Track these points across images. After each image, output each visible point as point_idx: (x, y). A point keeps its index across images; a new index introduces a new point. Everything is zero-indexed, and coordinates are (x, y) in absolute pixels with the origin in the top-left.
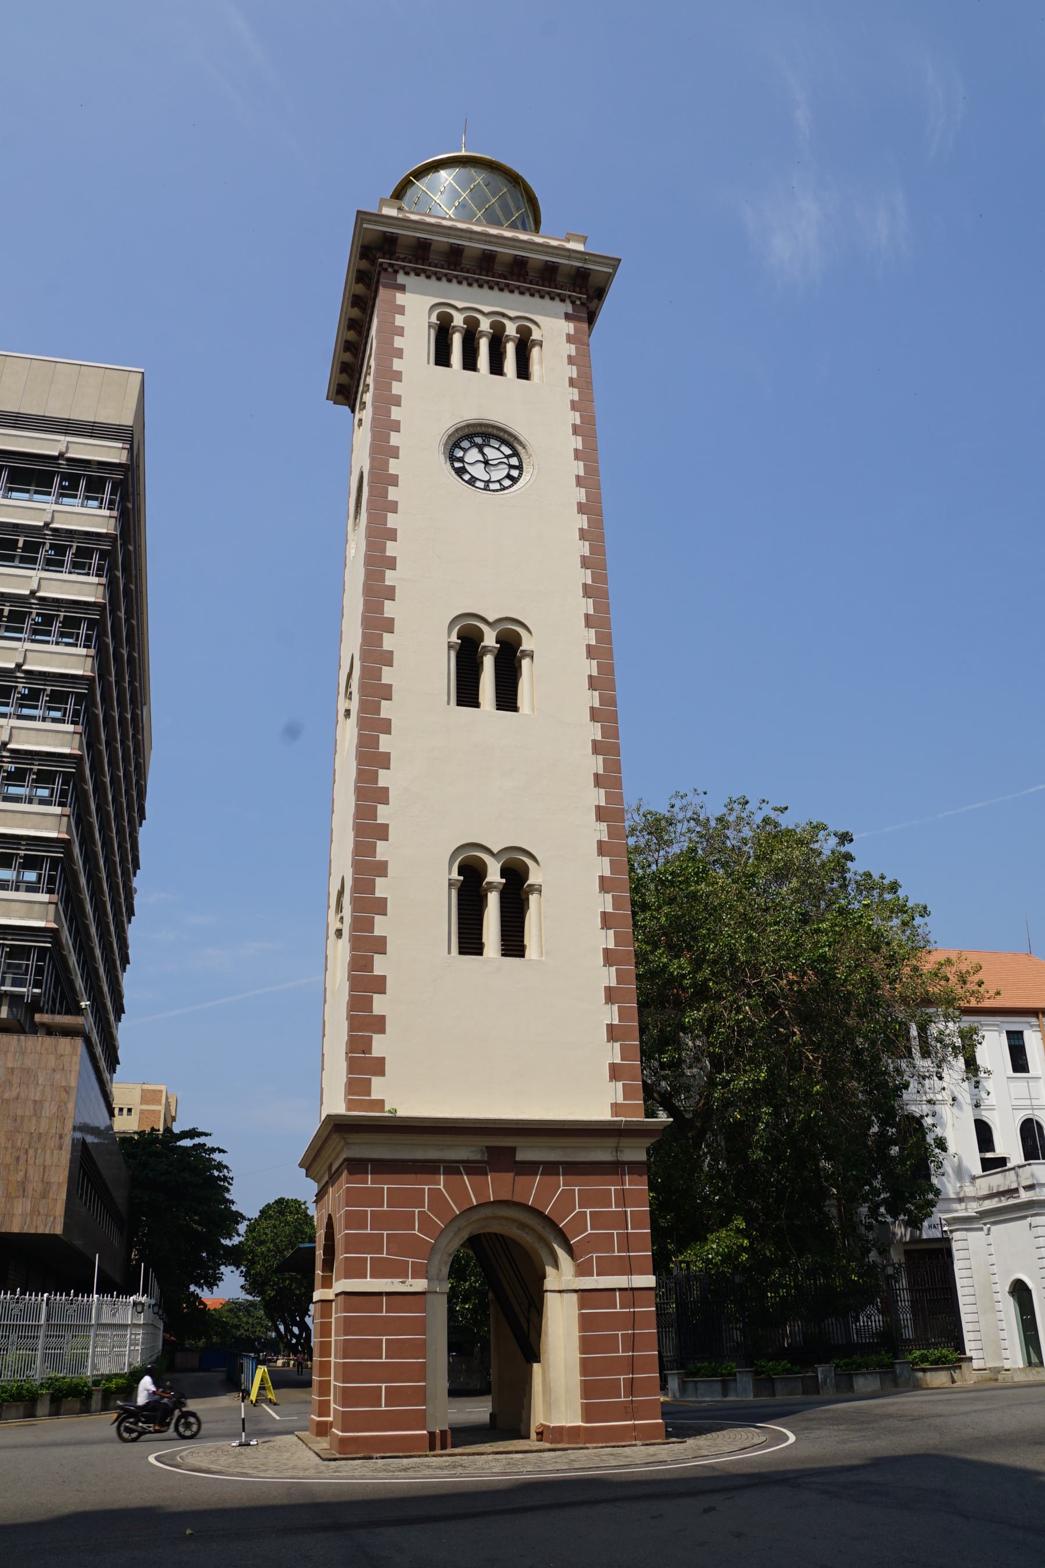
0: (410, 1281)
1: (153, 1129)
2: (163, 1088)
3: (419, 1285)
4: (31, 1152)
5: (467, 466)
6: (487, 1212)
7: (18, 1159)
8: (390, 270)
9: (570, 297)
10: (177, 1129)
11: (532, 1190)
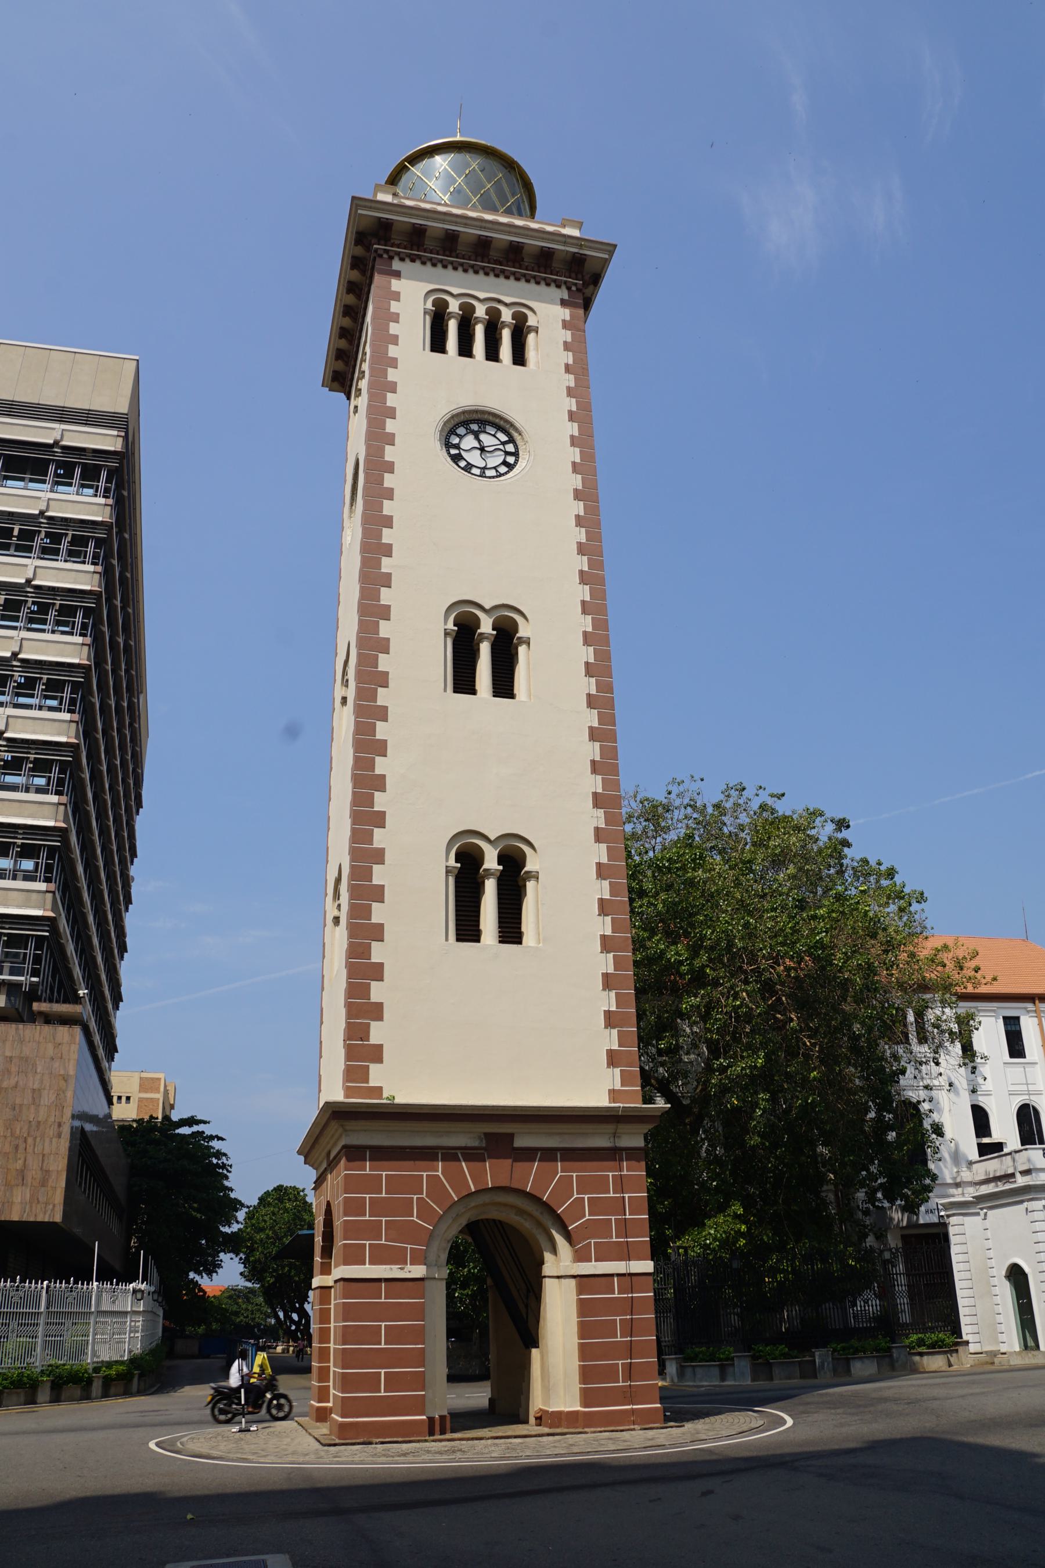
1: (151, 1117)
2: (161, 1076)
3: (418, 1271)
4: (30, 1140)
5: (463, 453)
6: (486, 1198)
7: (17, 1147)
8: (385, 256)
9: (565, 282)
10: (175, 1117)
11: (531, 1176)
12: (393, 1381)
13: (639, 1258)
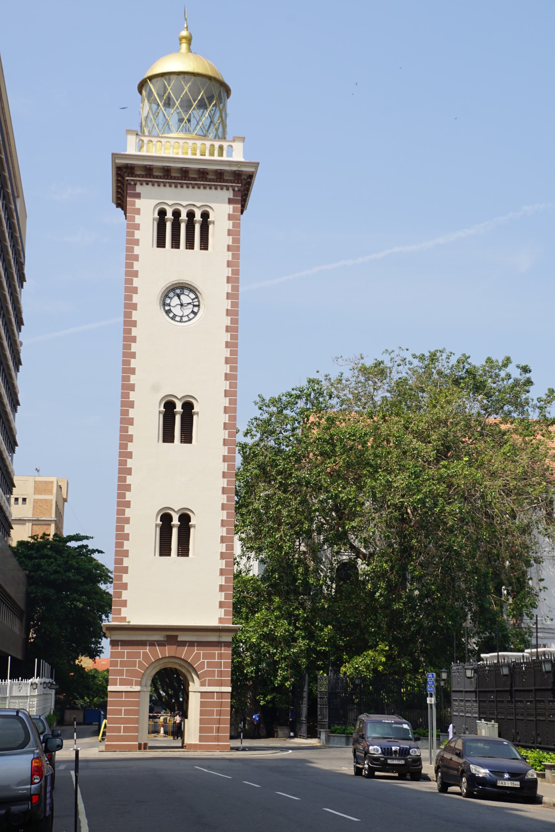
0: (134, 687)
1: (45, 534)
2: (54, 479)
3: (138, 688)
5: (172, 309)
6: (167, 660)
10: (65, 535)
11: (184, 652)
12: (126, 730)
13: (226, 686)
